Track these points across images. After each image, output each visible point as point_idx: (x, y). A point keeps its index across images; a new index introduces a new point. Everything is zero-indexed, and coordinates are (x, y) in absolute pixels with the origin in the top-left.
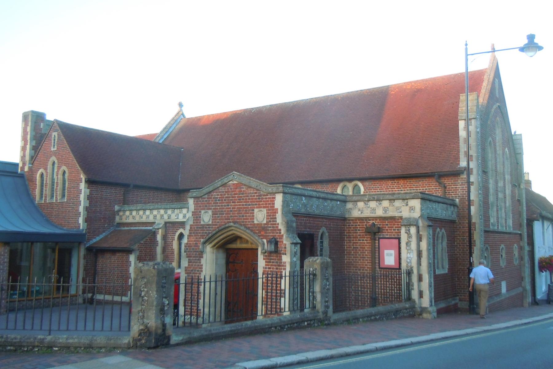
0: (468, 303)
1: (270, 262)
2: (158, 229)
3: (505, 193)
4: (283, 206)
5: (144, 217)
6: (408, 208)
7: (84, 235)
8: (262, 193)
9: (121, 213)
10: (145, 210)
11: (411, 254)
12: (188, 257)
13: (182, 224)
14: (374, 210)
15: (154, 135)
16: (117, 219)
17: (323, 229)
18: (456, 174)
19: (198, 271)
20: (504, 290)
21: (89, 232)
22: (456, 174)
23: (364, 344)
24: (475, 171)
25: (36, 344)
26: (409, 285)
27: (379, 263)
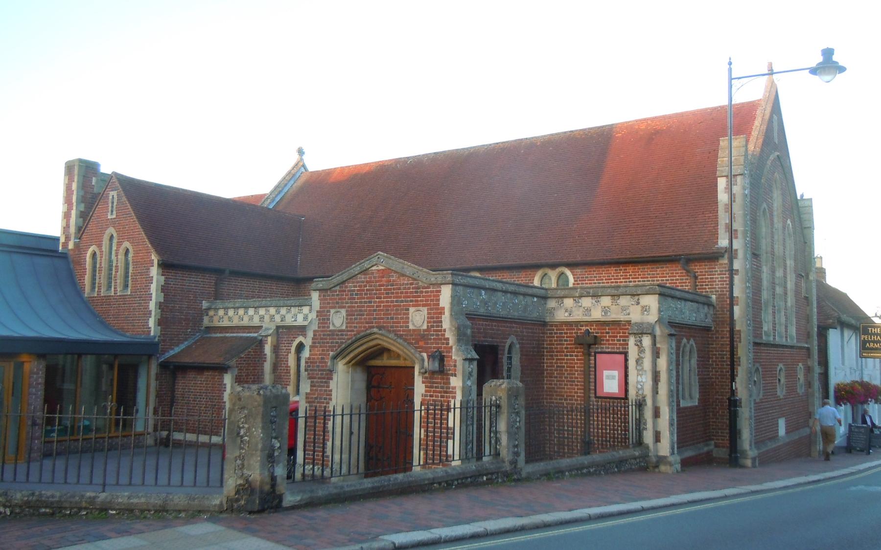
1: (432, 387)
2: (267, 336)
3: (785, 288)
4: (452, 303)
5: (246, 319)
6: (639, 308)
7: (156, 345)
8: (420, 284)
10: (246, 308)
11: (643, 378)
12: (309, 378)
13: (302, 330)
14: (588, 310)
15: (262, 196)
16: (206, 321)
17: (512, 339)
18: (713, 257)
19: (325, 399)
20: (782, 431)
21: (164, 341)
22: (713, 257)
23: (570, 510)
24: (740, 254)
25: (84, 504)
26: (640, 423)
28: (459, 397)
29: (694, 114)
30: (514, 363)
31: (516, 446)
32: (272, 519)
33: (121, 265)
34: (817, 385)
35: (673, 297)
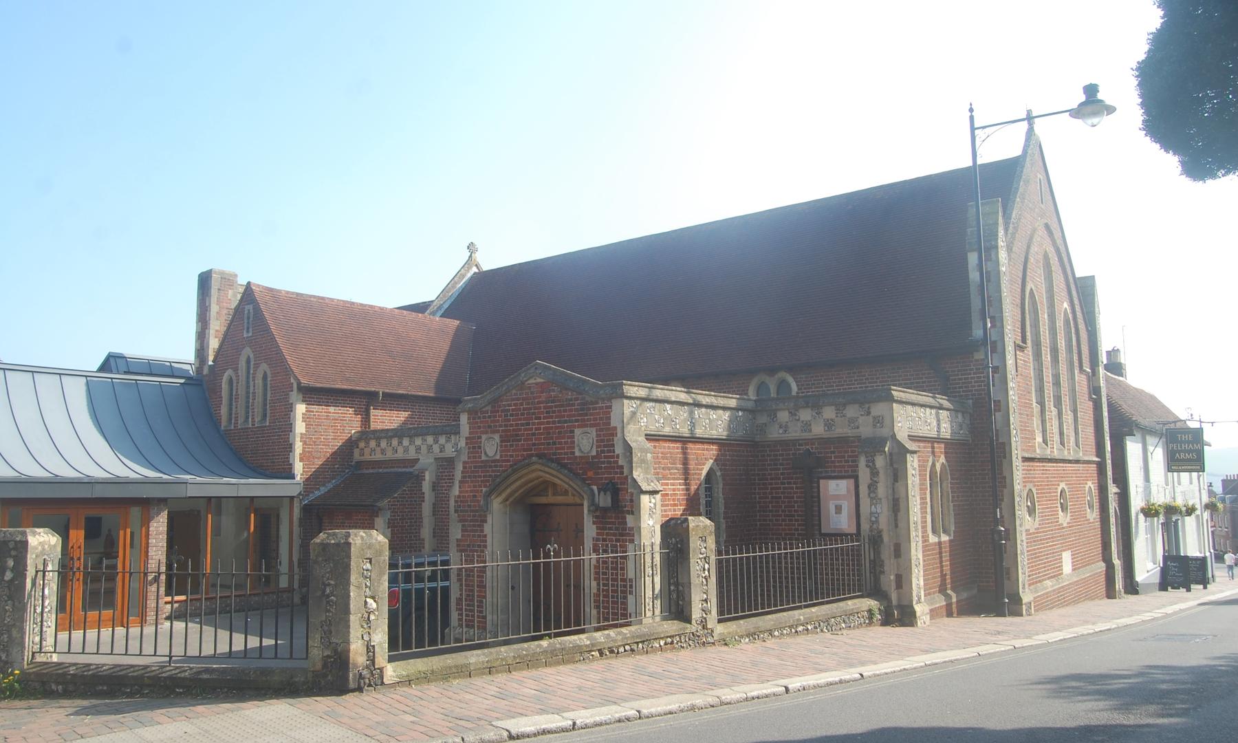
1: (604, 529)
5: (400, 450)
6: (870, 419)
12: (460, 521)
19: (479, 546)
20: (1067, 568)
29: (936, 175)
33: (259, 391)
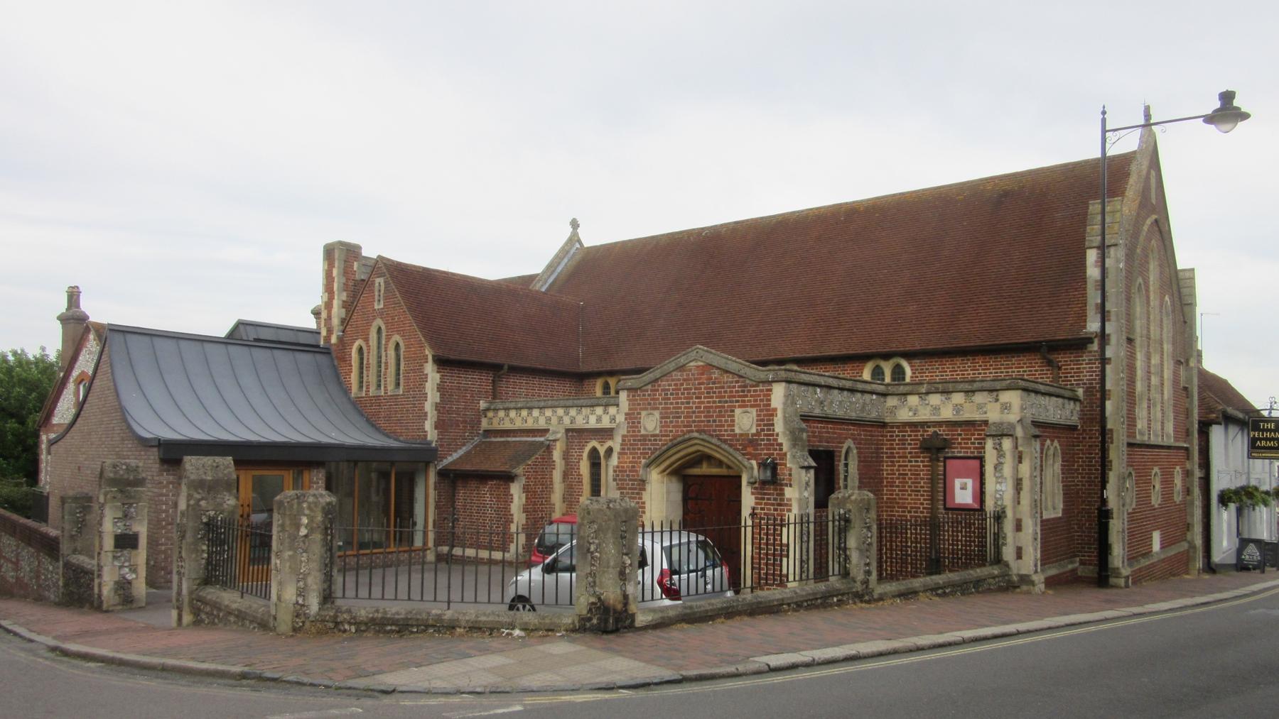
0: (1097, 569)
3: (1162, 377)
4: (785, 404)
7: (435, 450)
9: (490, 414)
11: (1014, 488)
13: (606, 433)
14: (936, 409)
15: (530, 279)
16: (485, 424)
17: (849, 443)
18: (1079, 344)
20: (1156, 546)
21: (442, 446)
22: (1079, 344)
23: (941, 633)
24: (1113, 340)
25: (431, 622)
26: (998, 538)
27: (945, 500)
28: (795, 510)
30: (850, 470)
31: (868, 564)
32: (630, 638)
33: (392, 362)
34: (1197, 491)
35: (1037, 392)
